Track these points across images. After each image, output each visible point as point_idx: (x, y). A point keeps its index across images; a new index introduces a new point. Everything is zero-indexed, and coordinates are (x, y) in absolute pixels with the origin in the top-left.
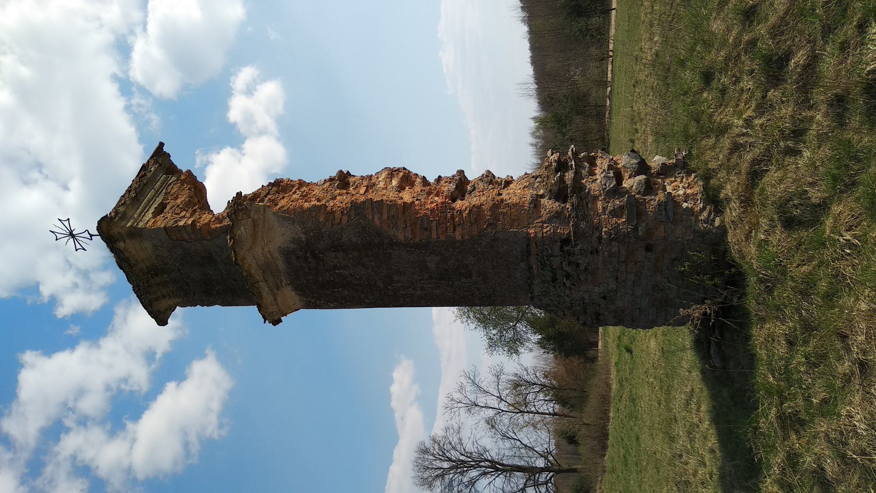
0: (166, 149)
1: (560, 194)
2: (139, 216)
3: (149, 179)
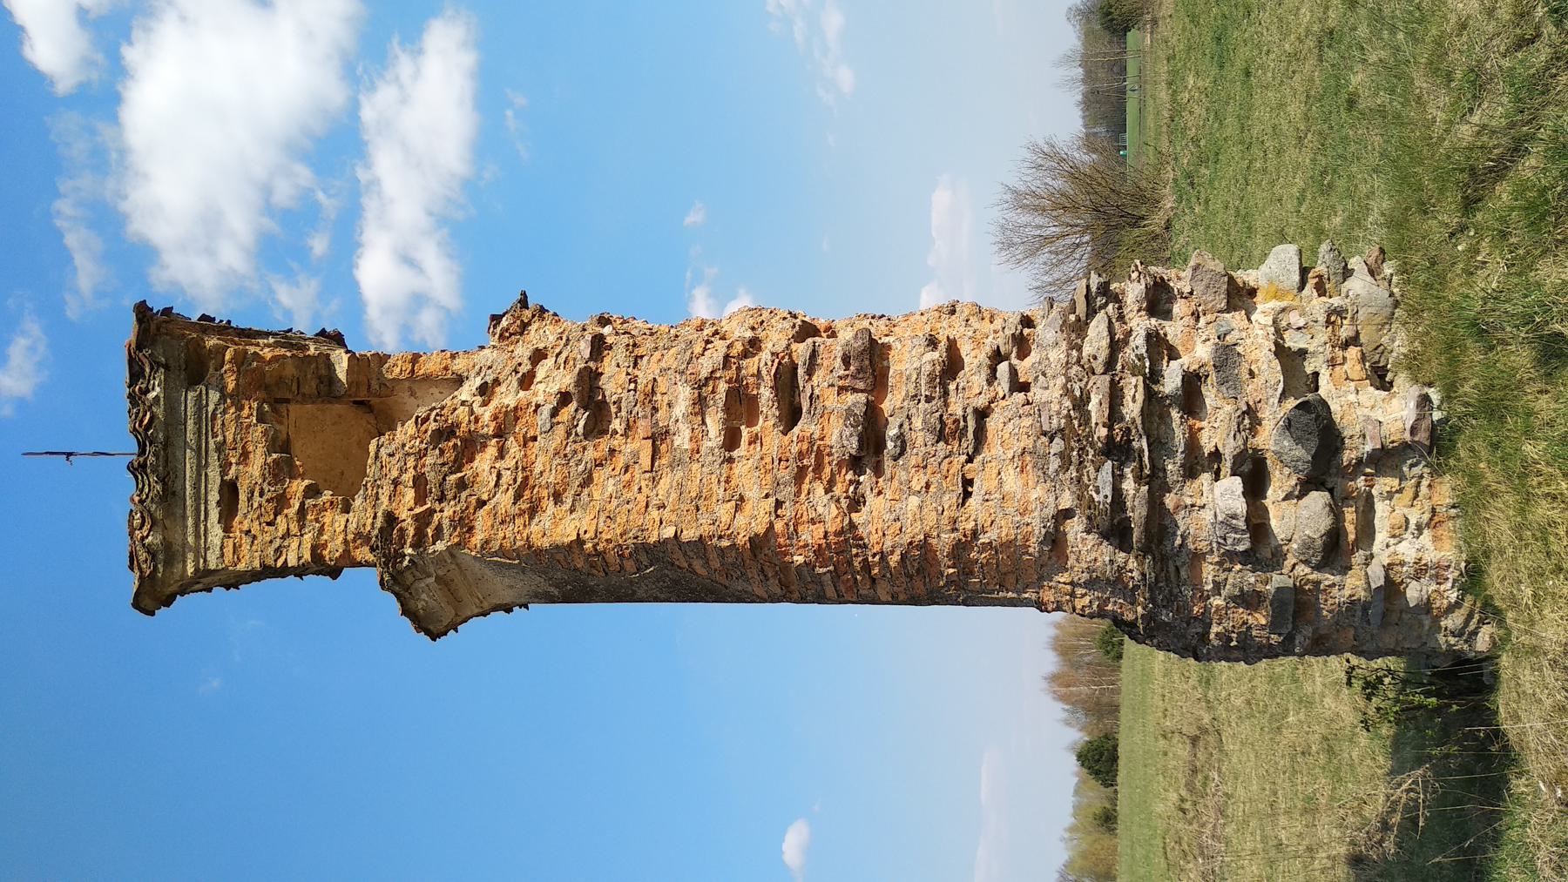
0: (157, 306)
1: (1115, 530)
2: (197, 536)
3: (167, 424)
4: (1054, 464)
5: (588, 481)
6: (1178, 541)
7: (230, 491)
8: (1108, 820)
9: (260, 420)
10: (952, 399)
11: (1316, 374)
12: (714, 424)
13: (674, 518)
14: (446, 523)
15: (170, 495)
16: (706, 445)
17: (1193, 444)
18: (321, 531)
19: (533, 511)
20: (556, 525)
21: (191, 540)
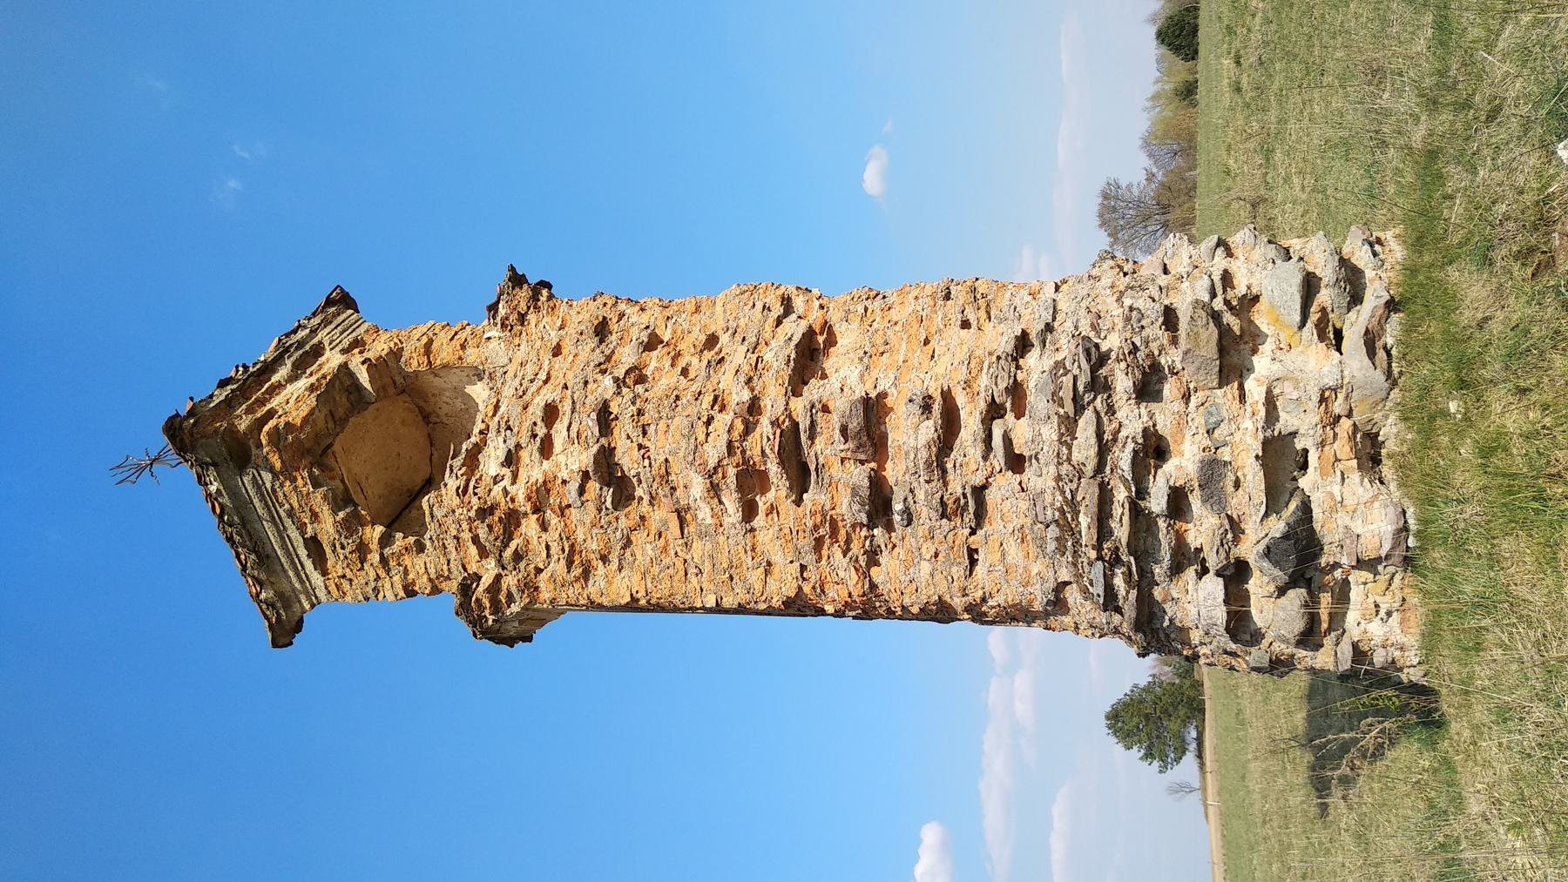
4: (1051, 546)
5: (628, 543)
6: (1166, 623)
7: (314, 545)
8: (1188, 92)
9: (316, 485)
10: (950, 477)
11: (1306, 451)
12: (731, 502)
13: (712, 587)
14: (514, 590)
15: (265, 559)
16: (727, 521)
17: (1180, 539)
18: (406, 572)
19: (586, 574)
20: (609, 583)
21: (297, 585)
